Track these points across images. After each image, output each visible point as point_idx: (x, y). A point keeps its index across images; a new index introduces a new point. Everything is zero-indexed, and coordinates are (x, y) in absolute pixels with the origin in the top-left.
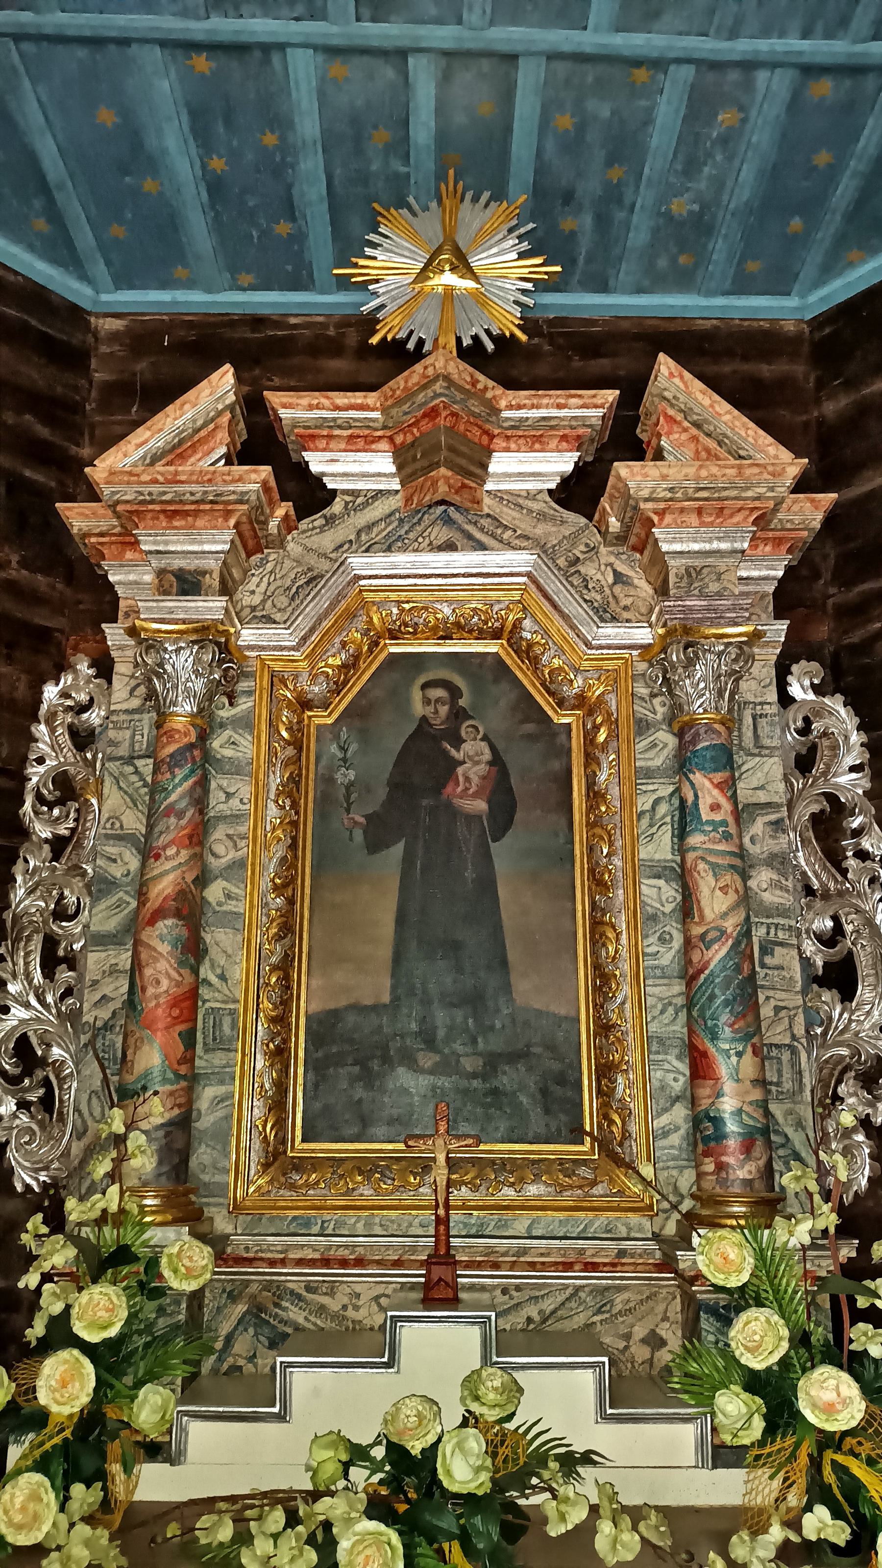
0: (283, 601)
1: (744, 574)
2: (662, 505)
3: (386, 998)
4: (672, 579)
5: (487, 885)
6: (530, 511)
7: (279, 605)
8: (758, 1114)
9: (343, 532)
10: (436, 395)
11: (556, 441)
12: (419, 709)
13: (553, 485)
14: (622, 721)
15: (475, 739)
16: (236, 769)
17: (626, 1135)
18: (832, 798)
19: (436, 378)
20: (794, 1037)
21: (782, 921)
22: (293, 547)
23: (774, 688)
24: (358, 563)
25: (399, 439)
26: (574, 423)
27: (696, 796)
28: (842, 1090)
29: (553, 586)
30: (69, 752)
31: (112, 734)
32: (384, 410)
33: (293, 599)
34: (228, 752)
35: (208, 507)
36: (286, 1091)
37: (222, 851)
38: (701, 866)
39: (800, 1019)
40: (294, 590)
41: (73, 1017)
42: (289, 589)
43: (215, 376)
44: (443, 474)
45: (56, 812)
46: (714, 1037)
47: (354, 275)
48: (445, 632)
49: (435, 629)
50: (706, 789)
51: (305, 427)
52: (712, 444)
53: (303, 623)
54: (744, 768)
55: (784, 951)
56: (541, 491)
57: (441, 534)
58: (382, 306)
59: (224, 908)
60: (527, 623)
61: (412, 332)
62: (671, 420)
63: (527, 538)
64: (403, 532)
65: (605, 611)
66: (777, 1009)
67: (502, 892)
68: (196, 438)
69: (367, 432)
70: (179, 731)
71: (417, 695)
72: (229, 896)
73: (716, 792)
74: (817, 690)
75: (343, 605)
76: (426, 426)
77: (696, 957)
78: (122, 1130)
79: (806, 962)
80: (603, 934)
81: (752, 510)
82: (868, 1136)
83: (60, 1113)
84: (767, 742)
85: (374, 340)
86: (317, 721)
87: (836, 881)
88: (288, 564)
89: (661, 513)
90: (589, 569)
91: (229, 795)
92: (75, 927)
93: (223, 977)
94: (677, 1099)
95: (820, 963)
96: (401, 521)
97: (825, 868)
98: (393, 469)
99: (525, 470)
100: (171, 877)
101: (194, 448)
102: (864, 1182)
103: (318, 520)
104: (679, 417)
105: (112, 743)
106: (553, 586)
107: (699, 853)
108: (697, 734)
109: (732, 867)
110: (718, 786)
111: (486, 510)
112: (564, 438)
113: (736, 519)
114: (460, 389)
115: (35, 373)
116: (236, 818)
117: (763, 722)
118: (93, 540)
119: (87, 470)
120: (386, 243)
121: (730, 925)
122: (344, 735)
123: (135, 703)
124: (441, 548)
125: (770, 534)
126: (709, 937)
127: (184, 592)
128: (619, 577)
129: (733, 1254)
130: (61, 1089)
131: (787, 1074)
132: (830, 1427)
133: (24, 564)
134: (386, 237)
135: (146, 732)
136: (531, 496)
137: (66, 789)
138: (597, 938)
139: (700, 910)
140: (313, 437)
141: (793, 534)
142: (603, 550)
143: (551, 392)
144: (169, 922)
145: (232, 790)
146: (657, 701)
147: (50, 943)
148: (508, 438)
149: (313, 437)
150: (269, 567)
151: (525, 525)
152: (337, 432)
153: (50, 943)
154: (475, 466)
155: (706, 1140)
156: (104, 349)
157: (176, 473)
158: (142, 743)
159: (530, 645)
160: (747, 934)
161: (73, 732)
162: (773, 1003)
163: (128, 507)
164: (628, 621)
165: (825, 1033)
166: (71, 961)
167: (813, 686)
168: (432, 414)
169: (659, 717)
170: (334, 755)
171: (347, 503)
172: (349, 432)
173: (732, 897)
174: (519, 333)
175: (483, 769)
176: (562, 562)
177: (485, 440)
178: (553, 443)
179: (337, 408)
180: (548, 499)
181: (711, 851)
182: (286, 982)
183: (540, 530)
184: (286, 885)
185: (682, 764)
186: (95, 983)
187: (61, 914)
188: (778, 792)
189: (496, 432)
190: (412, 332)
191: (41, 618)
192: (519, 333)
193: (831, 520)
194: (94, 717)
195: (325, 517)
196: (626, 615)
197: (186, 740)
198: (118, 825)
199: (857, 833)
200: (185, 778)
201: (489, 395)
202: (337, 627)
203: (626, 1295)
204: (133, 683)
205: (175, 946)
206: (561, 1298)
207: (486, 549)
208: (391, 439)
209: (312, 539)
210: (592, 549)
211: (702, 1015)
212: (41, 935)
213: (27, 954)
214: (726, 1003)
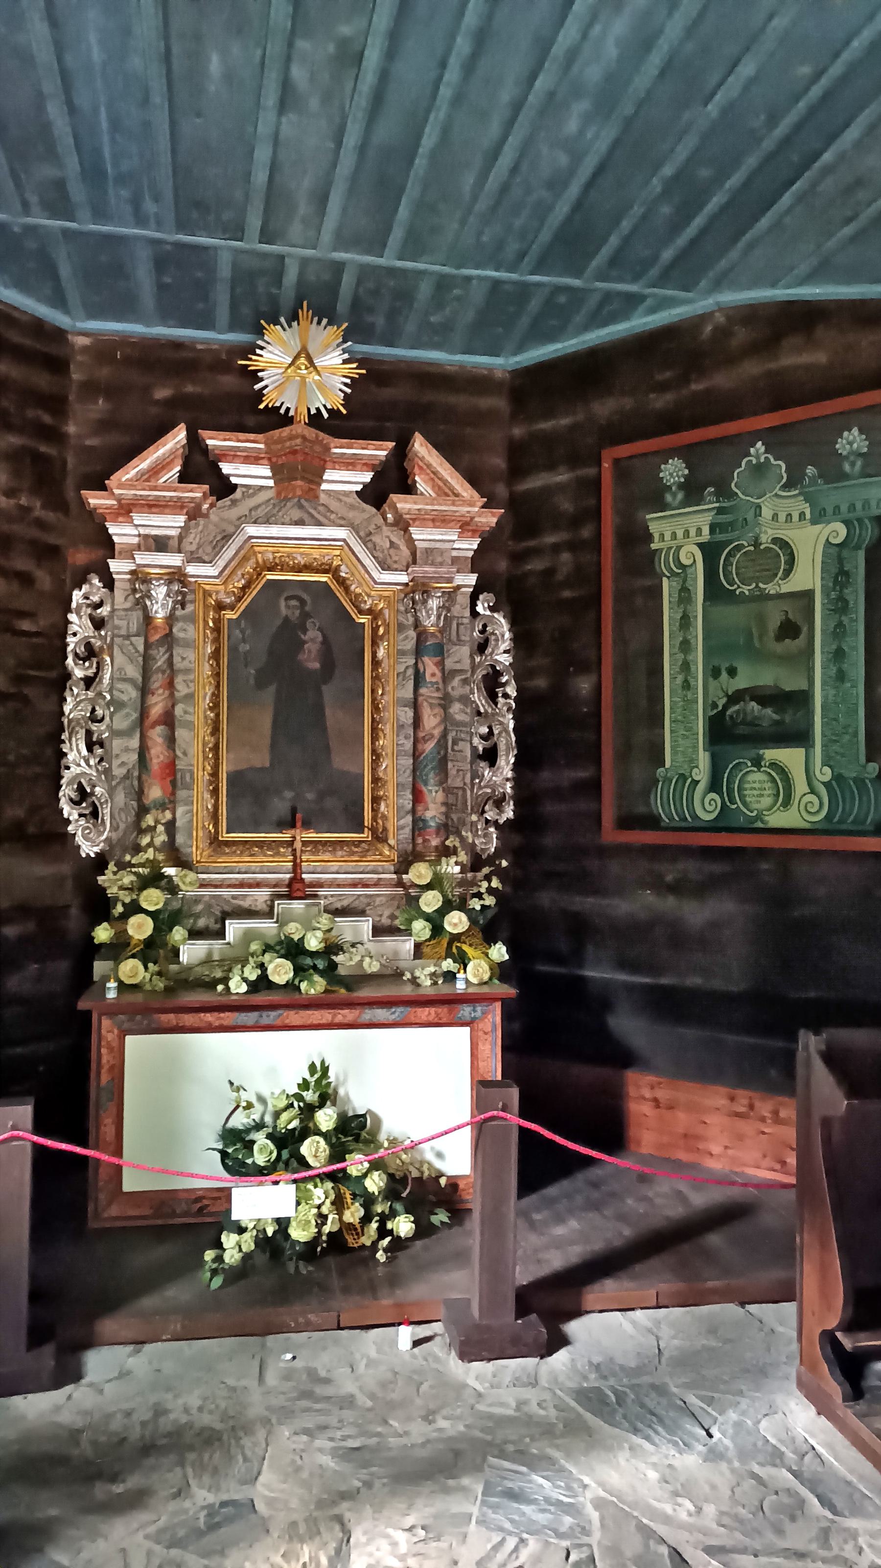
0: (209, 549)
2: (414, 517)
3: (267, 765)
5: (319, 709)
6: (345, 503)
8: (443, 818)
14: (392, 626)
16: (187, 644)
17: (385, 829)
18: (493, 667)
20: (465, 784)
21: (464, 729)
22: (213, 517)
23: (468, 609)
24: (252, 530)
29: (358, 548)
30: (90, 631)
31: (117, 622)
32: (266, 444)
34: (181, 635)
36: (218, 809)
37: (182, 689)
38: (425, 704)
39: (469, 775)
41: (107, 772)
42: (212, 542)
44: (298, 478)
45: (87, 664)
46: (426, 784)
47: (250, 366)
48: (299, 569)
49: (293, 567)
50: (430, 666)
53: (221, 563)
55: (463, 743)
56: (351, 492)
57: (296, 514)
58: (266, 386)
60: (343, 568)
61: (282, 403)
62: (421, 468)
63: (343, 518)
64: (275, 511)
65: (385, 563)
66: (458, 771)
67: (328, 712)
71: (282, 603)
72: (186, 712)
73: (434, 667)
74: (492, 609)
75: (242, 552)
76: (291, 457)
77: (420, 747)
78: (153, 824)
79: (474, 749)
80: (377, 734)
82: (496, 829)
83: (103, 820)
84: (463, 638)
85: (262, 406)
86: (228, 616)
88: (211, 527)
89: (414, 520)
90: (376, 539)
91: (183, 659)
92: (103, 726)
95: (481, 749)
96: (274, 504)
97: (486, 702)
98: (270, 474)
99: (344, 481)
102: (493, 850)
103: (226, 501)
104: (425, 467)
105: (118, 628)
106: (358, 548)
109: (439, 705)
111: (322, 501)
114: (310, 441)
115: (42, 380)
116: (187, 671)
117: (462, 627)
118: (101, 511)
119: (106, 482)
120: (270, 348)
121: (437, 732)
122: (243, 625)
123: (128, 605)
126: (427, 738)
128: (392, 543)
129: (423, 872)
130: (102, 808)
132: (455, 932)
133: (43, 507)
134: (268, 343)
136: (347, 494)
137: (90, 653)
138: (374, 738)
140: (225, 455)
142: (385, 528)
144: (162, 727)
146: (409, 615)
147: (89, 733)
150: (200, 528)
151: (343, 511)
152: (239, 453)
153: (89, 733)
154: (317, 477)
155: (420, 829)
156: (79, 358)
158: (134, 628)
159: (344, 579)
161: (92, 618)
162: (456, 768)
165: (480, 782)
166: (101, 744)
167: (489, 606)
168: (294, 452)
171: (243, 493)
173: (438, 719)
174: (342, 409)
177: (322, 463)
178: (359, 467)
179: (239, 441)
180: (356, 496)
181: (431, 697)
182: (217, 757)
184: (215, 706)
185: (419, 651)
186: (117, 756)
187: (94, 719)
188: (466, 664)
190: (282, 403)
191: (52, 539)
192: (342, 409)
194: (104, 611)
201: (325, 442)
202: (240, 565)
203: (381, 898)
204: (126, 593)
208: (269, 459)
209: (222, 512)
210: (378, 527)
211: (421, 774)
212: (84, 731)
213: (77, 740)
214: (432, 768)
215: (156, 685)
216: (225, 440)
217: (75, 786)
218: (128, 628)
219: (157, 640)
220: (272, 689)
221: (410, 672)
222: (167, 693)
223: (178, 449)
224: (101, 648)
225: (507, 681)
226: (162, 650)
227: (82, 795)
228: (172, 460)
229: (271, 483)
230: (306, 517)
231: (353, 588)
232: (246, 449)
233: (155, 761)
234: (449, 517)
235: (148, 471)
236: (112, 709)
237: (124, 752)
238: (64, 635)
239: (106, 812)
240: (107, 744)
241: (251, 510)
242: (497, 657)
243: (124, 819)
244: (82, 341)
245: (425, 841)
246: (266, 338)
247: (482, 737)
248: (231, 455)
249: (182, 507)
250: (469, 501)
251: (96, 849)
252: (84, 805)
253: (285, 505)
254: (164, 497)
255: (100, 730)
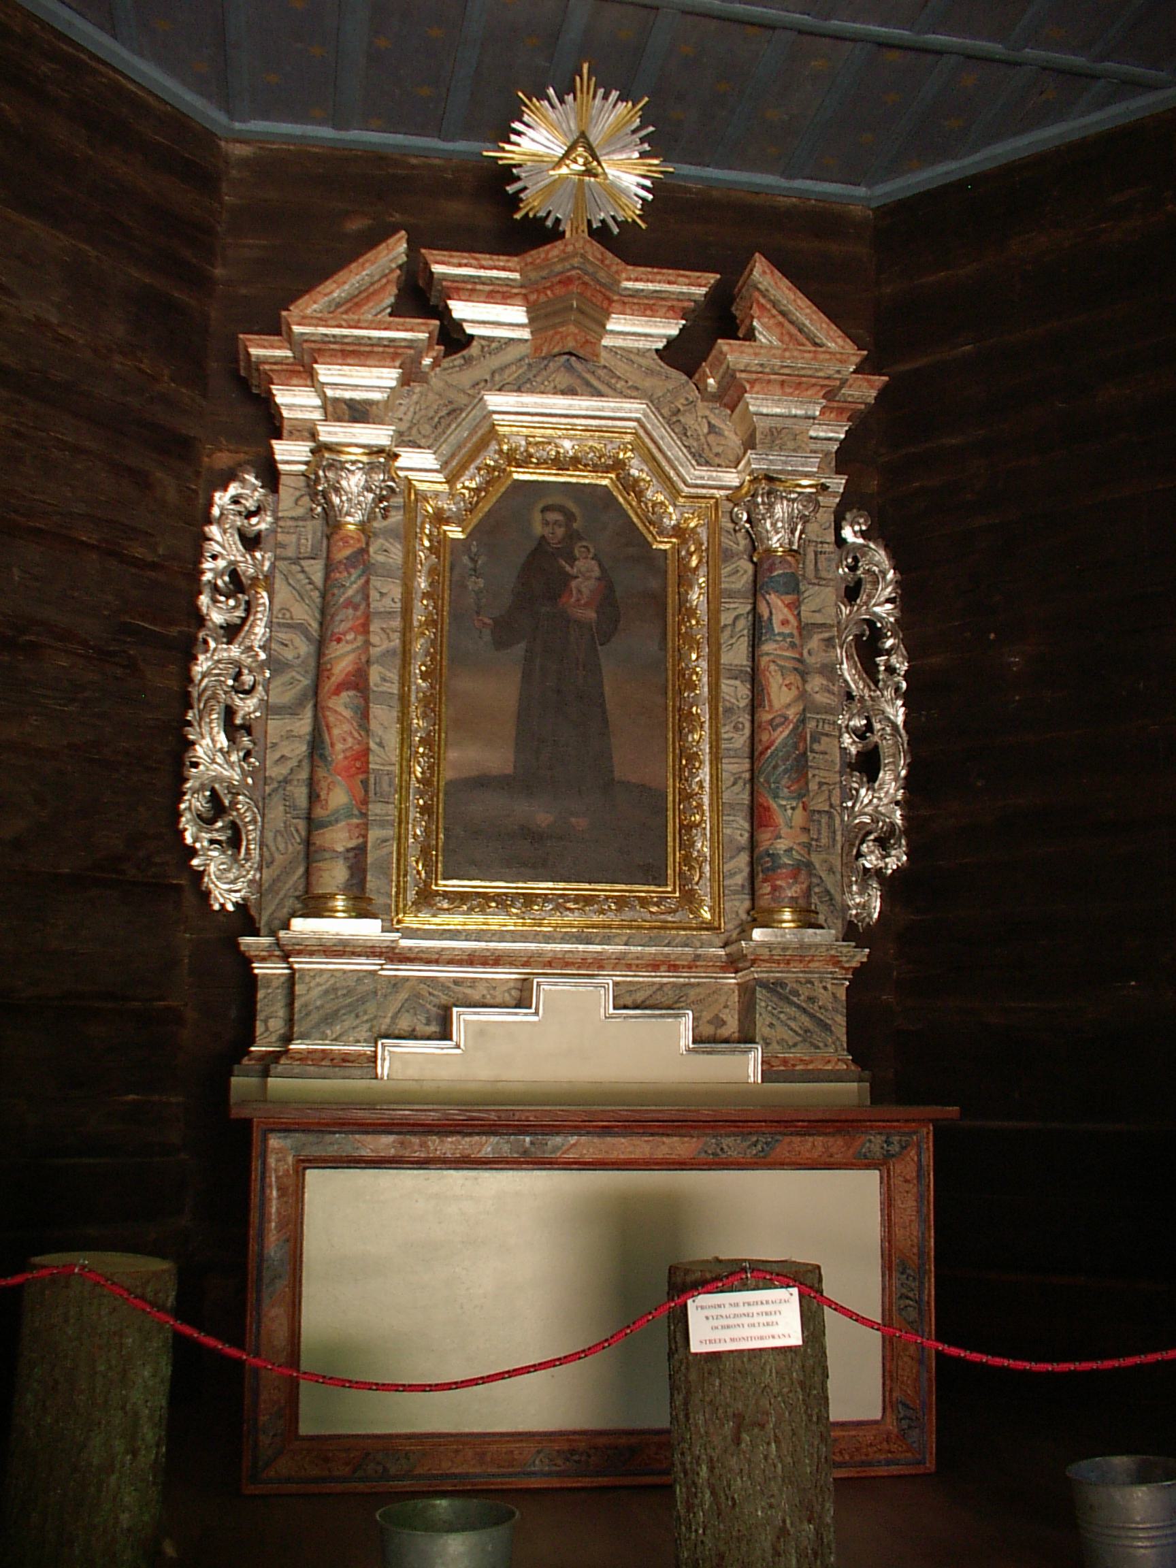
0: (427, 429)
1: (812, 433)
2: (754, 376)
4: (758, 436)
7: (423, 432)
9: (479, 371)
10: (574, 268)
11: (664, 310)
12: (538, 529)
13: (660, 345)
15: (586, 558)
18: (870, 623)
19: (575, 255)
20: (831, 806)
25: (533, 297)
26: (681, 297)
27: (771, 613)
28: (864, 848)
32: (521, 272)
33: (436, 427)
34: (381, 558)
35: (381, 349)
38: (772, 667)
39: (837, 792)
40: (436, 419)
42: (432, 418)
43: (391, 241)
47: (501, 158)
50: (777, 608)
51: (454, 281)
52: (794, 330)
54: (806, 594)
57: (563, 379)
59: (380, 689)
62: (762, 307)
63: (637, 389)
64: (531, 376)
65: (700, 456)
66: (820, 784)
68: (371, 290)
69: (505, 289)
70: (352, 538)
71: (537, 517)
73: (786, 610)
76: (559, 290)
79: (844, 750)
81: (823, 386)
84: (823, 574)
87: (870, 690)
88: (431, 396)
89: (752, 383)
93: (381, 745)
94: (742, 849)
97: (861, 678)
98: (525, 320)
99: (637, 331)
100: (351, 657)
101: (368, 299)
103: (457, 359)
106: (663, 434)
107: (772, 657)
108: (773, 564)
109: (796, 669)
110: (788, 606)
111: (603, 362)
112: (672, 308)
113: (809, 393)
117: (822, 558)
118: (267, 367)
119: (284, 313)
121: (792, 713)
123: (300, 511)
124: (563, 393)
125: (835, 405)
127: (355, 420)
128: (712, 428)
131: (824, 832)
135: (310, 537)
136: (639, 352)
139: (770, 701)
140: (458, 289)
141: (853, 406)
142: (700, 404)
143: (665, 271)
144: (351, 693)
145: (384, 591)
146: (738, 535)
148: (624, 303)
149: (458, 289)
150: (415, 397)
151: (635, 378)
152: (479, 287)
153: (230, 712)
156: (234, 173)
157: (359, 321)
159: (637, 481)
160: (803, 721)
162: (817, 779)
163: (313, 345)
164: (719, 466)
165: (853, 806)
169: (741, 548)
170: (465, 565)
171: (483, 347)
172: (491, 288)
173: (794, 692)
175: (592, 583)
176: (665, 411)
180: (656, 357)
183: (648, 383)
185: (757, 589)
186: (274, 745)
189: (616, 298)
193: (883, 393)
194: (261, 524)
195: (464, 357)
196: (717, 461)
197: (358, 545)
198: (288, 615)
199: (888, 652)
200: (359, 577)
203: (698, 990)
204: (298, 493)
205: (356, 713)
206: (649, 992)
207: (603, 396)
208: (525, 297)
211: (767, 781)
214: (786, 771)
215: (343, 627)
216: (460, 265)
217: (208, 793)
218: (298, 546)
219: (347, 558)
220: (520, 649)
221: (742, 624)
222: (360, 638)
223: (392, 271)
224: (255, 579)
225: (892, 648)
226: (355, 573)
227: (217, 807)
228: (383, 288)
229: (525, 334)
230: (577, 384)
231: (649, 493)
232: (491, 281)
233: (339, 746)
234: (802, 380)
235: (347, 301)
236: (268, 675)
237: (288, 737)
238: (198, 556)
239: (251, 834)
240: (257, 731)
241: (493, 374)
242: (877, 609)
243: (282, 847)
244: (241, 150)
245: (775, 888)
246: (526, 118)
247: (855, 731)
248: (471, 290)
249: (395, 356)
250: (838, 350)
251: (236, 897)
252: (219, 824)
253: (546, 367)
254: (369, 338)
255: (247, 706)
